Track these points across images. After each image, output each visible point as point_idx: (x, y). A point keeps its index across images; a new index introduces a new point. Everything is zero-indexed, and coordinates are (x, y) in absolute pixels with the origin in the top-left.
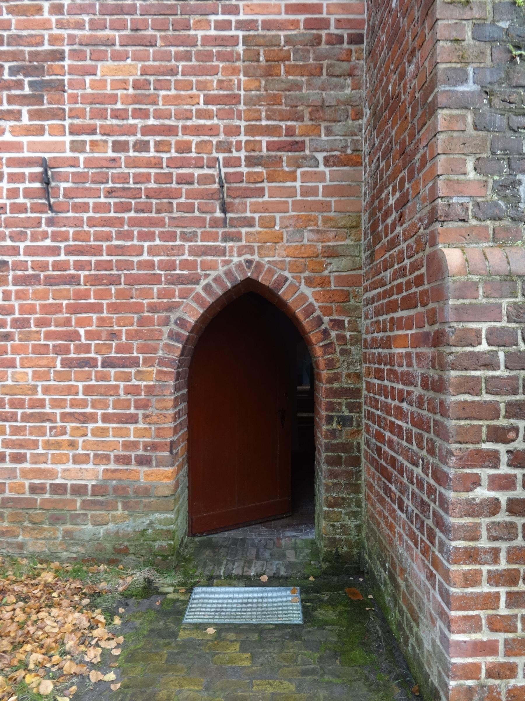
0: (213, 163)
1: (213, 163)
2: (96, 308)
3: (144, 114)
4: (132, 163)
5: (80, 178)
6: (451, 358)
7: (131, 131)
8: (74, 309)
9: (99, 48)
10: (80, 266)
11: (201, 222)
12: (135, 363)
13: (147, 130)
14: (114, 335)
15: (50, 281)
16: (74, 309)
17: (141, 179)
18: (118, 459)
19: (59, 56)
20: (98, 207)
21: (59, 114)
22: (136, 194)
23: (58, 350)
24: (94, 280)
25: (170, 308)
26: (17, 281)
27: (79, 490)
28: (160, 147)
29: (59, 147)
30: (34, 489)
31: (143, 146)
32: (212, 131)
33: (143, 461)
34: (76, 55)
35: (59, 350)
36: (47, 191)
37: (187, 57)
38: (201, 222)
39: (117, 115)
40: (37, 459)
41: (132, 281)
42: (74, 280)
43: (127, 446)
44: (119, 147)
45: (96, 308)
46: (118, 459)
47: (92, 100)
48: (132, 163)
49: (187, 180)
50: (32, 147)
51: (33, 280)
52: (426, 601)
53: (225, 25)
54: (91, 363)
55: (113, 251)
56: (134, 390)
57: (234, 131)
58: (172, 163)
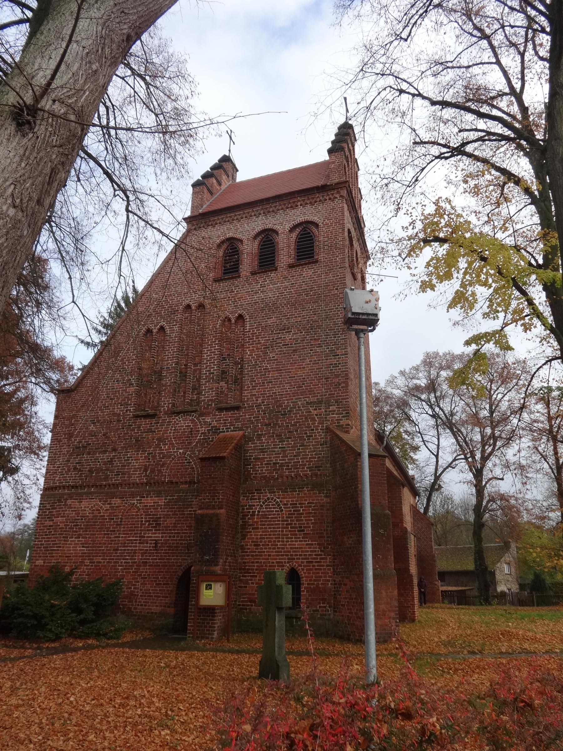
0: (187, 540)
1: (187, 540)
2: (163, 572)
3: (174, 530)
4: (172, 540)
5: (162, 543)
6: (364, 696)
7: (172, 533)
8: (159, 572)
9: (167, 516)
10: (161, 562)
11: (183, 553)
12: (168, 584)
13: (175, 533)
14: (165, 578)
15: (155, 566)
16: (159, 572)
17: (173, 543)
18: (165, 606)
19: (160, 518)
20: (165, 550)
21: (159, 530)
22: (172, 547)
23: (155, 581)
24: (162, 566)
25: (177, 572)
26: (149, 566)
27: (156, 613)
28: (178, 537)
29: (159, 537)
30: (148, 613)
31: (174, 537)
32: (187, 533)
33: (169, 607)
34: (164, 518)
35: (155, 581)
36: (156, 547)
37: (183, 518)
38: (183, 553)
39: (170, 530)
40: (149, 606)
41: (170, 566)
42: (159, 566)
43: (166, 603)
44: (170, 537)
45: (163, 572)
46: (165, 606)
47: (165, 527)
48: (172, 540)
49: (182, 544)
50: (154, 537)
51: (151, 566)
52: (352, 230)
53: (190, 511)
54: (161, 584)
55: (167, 559)
56: (168, 590)
57: (191, 533)
58: (180, 540)
